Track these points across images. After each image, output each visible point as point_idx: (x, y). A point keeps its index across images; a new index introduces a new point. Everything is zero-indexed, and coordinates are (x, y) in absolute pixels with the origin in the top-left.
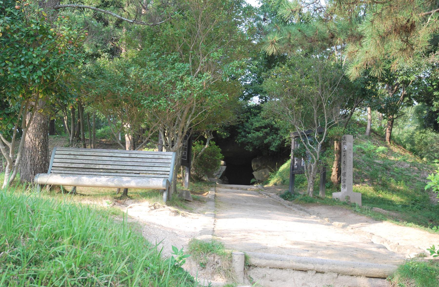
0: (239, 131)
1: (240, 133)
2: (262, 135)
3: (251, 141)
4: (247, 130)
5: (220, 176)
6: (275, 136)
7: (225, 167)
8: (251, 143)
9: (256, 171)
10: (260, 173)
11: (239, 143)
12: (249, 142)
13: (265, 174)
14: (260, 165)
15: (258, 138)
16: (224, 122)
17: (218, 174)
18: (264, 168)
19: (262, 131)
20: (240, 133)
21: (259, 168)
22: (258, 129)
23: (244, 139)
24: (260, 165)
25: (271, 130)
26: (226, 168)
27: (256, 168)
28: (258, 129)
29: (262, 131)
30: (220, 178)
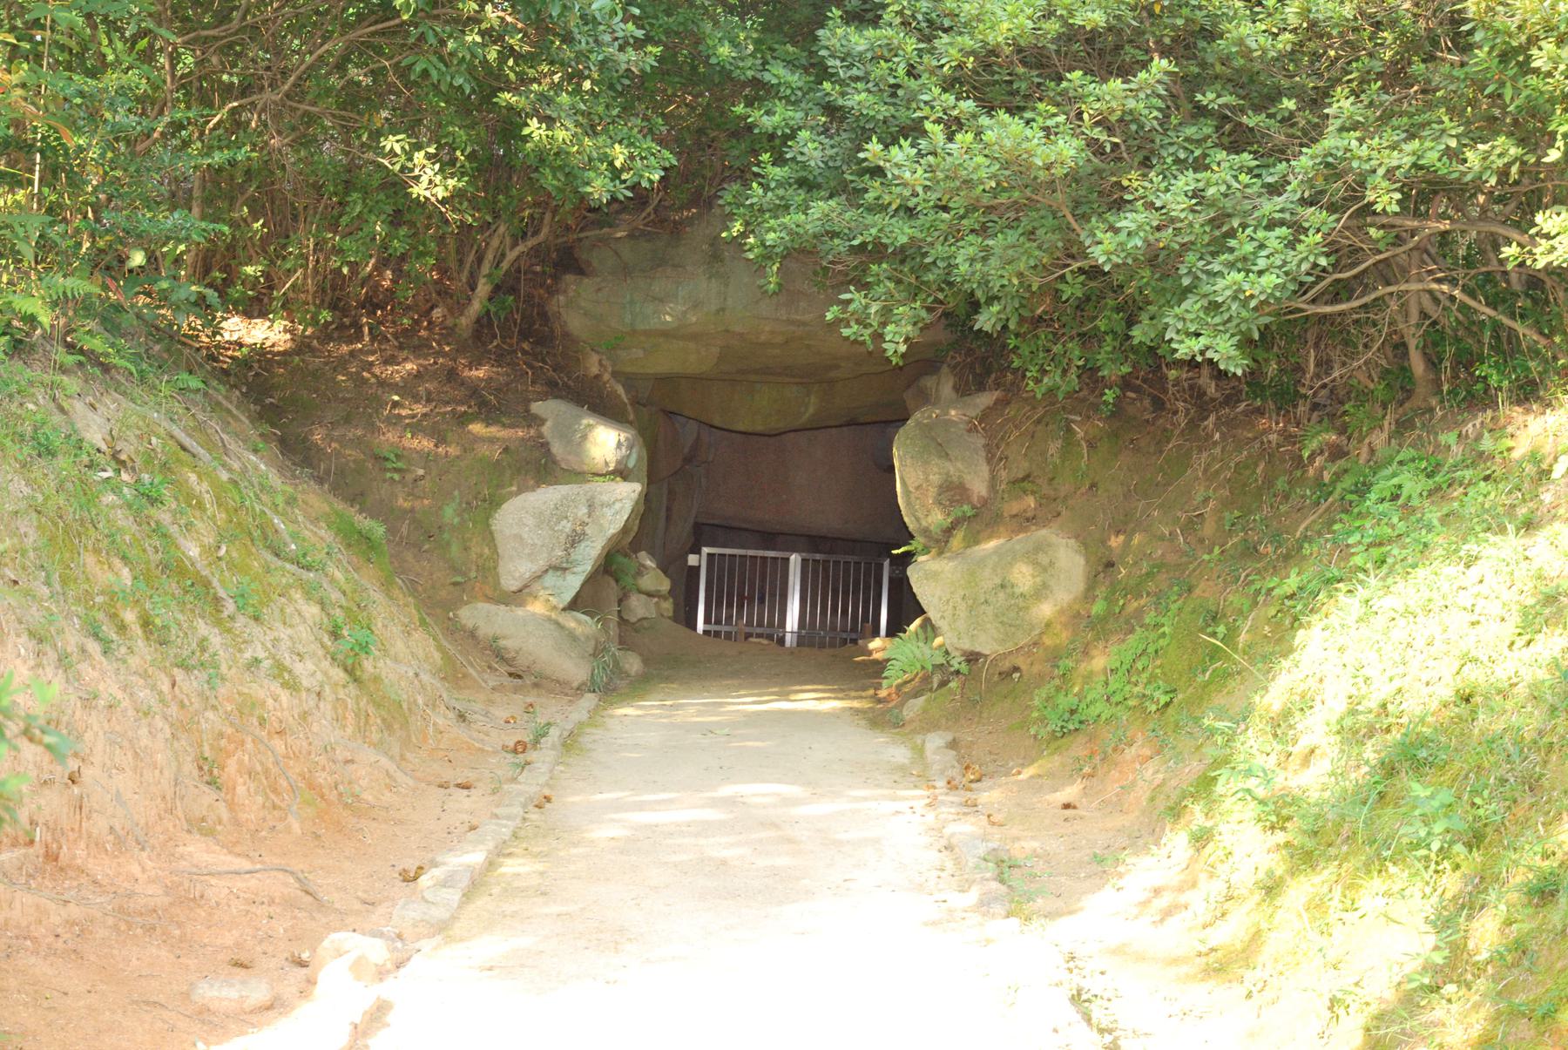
0: (769, 119)
1: (778, 143)
2: (1068, 150)
3: (901, 233)
4: (858, 99)
5: (573, 583)
6: (1226, 172)
7: (624, 497)
8: (902, 255)
9: (940, 542)
10: (988, 580)
11: (768, 254)
12: (875, 251)
13: (1041, 592)
14: (978, 486)
15: (1015, 201)
16: (1221, 781)
17: (560, 569)
18: (1026, 521)
19: (1068, 101)
20: (778, 143)
21: (973, 519)
22: (1002, 81)
23: (819, 208)
24: (978, 486)
25: (1182, 95)
26: (647, 498)
27: (937, 519)
28: (1002, 81)
29: (1068, 101)
30: (574, 605)
